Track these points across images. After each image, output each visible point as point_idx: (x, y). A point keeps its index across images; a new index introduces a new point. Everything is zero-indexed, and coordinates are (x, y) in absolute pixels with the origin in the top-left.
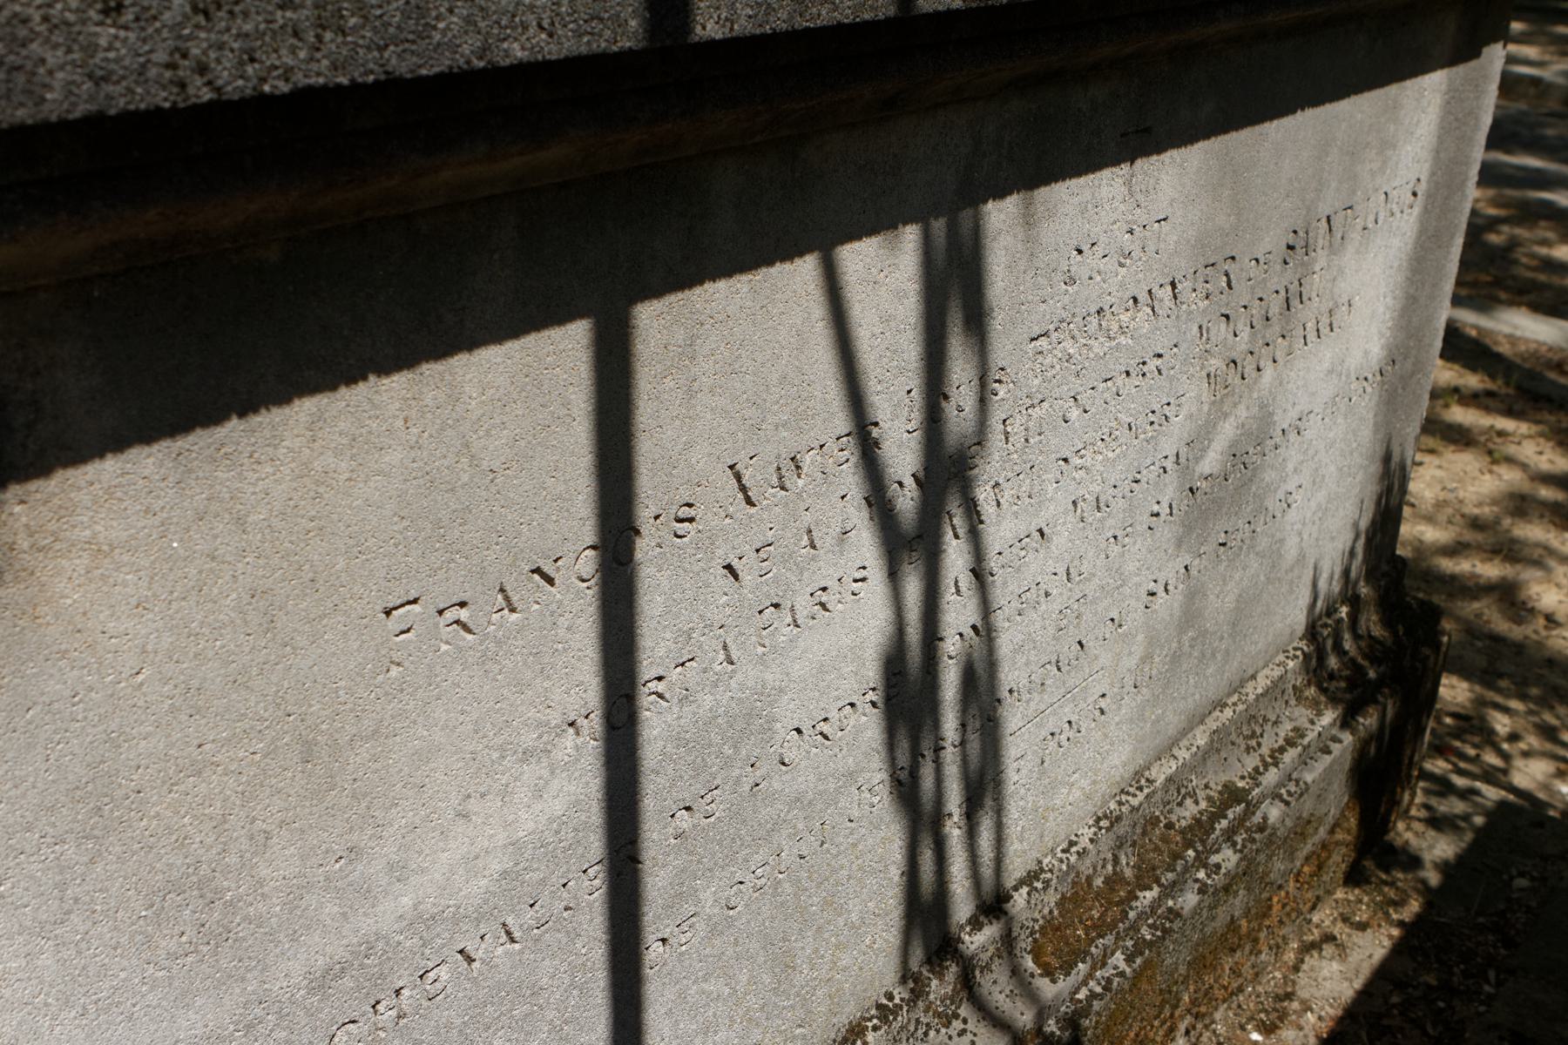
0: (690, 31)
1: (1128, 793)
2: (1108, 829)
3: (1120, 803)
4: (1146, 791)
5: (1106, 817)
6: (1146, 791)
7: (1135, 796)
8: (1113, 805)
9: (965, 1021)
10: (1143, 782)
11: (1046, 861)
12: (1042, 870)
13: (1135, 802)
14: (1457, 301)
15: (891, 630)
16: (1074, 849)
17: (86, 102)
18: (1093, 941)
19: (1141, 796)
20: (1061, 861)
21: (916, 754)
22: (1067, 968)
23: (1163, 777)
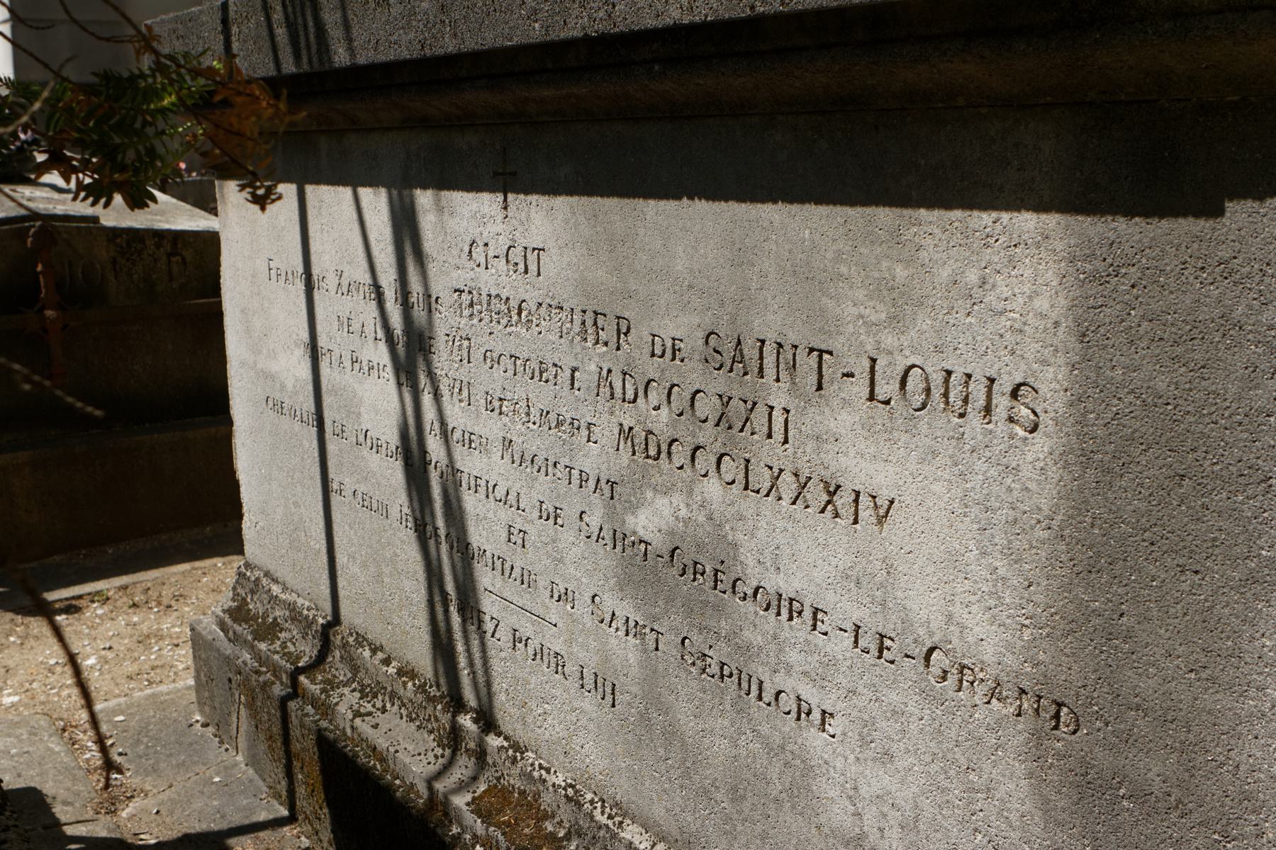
0: (1231, 200)
1: (603, 807)
2: (566, 796)
3: (592, 802)
4: (610, 823)
5: (577, 792)
6: (610, 823)
7: (603, 813)
8: (589, 796)
9: (443, 756)
10: (618, 819)
11: (530, 754)
12: (522, 753)
13: (597, 813)
14: (209, 244)
15: (401, 419)
16: (543, 772)
17: (146, 148)
18: (499, 828)
19: (603, 819)
20: (532, 765)
21: (422, 511)
22: (478, 812)
23: (629, 837)
